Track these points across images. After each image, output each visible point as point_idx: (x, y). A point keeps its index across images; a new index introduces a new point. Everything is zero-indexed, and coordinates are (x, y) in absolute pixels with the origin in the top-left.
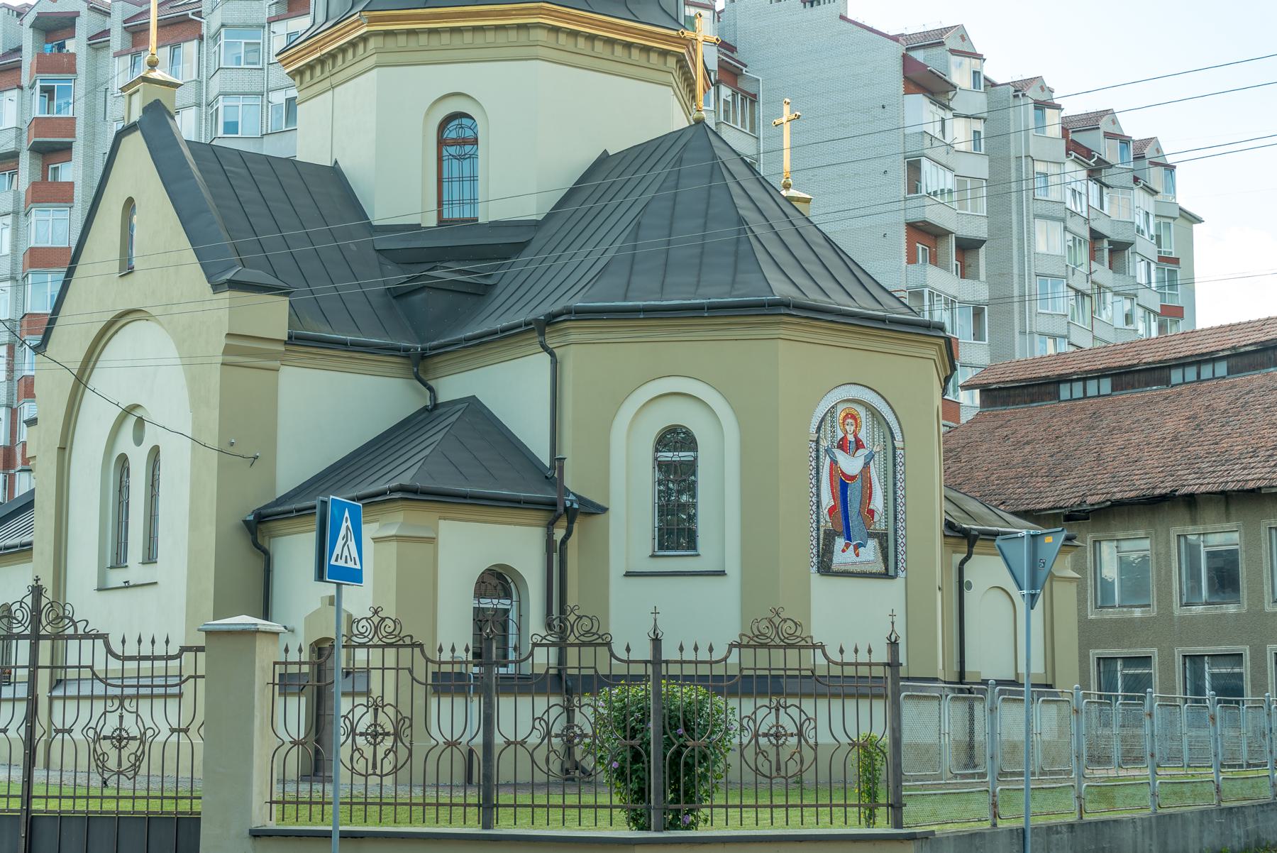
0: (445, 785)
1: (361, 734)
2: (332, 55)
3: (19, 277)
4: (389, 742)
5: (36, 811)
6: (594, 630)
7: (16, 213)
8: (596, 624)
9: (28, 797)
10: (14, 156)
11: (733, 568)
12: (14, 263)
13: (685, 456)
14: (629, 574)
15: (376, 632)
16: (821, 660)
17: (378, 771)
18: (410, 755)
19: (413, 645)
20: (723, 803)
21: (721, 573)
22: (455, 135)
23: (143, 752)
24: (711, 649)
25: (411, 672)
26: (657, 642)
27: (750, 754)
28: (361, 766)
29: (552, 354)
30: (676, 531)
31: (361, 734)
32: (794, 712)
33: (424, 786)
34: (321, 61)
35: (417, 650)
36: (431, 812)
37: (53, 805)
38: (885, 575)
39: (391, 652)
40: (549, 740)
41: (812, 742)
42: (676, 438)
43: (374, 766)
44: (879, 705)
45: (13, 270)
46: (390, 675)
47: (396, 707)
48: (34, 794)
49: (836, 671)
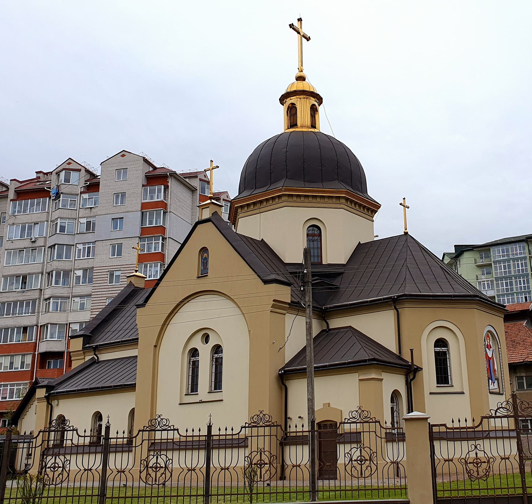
2: (261, 202)
4: (162, 470)
5: (439, 498)
6: (167, 424)
8: (369, 413)
9: (524, 487)
11: (466, 391)
13: (444, 349)
14: (431, 393)
15: (360, 416)
16: (177, 436)
17: (363, 476)
18: (171, 475)
19: (174, 430)
21: (463, 393)
22: (315, 233)
23: (489, 467)
24: (232, 429)
25: (276, 436)
26: (210, 427)
27: (348, 468)
28: (355, 473)
29: (397, 311)
30: (443, 376)
32: (164, 457)
34: (254, 204)
35: (176, 432)
37: (447, 494)
38: (499, 394)
39: (267, 429)
40: (147, 469)
41: (375, 462)
42: (441, 343)
43: (361, 474)
44: (306, 449)
46: (267, 438)
47: (270, 452)
48: (527, 486)
49: (184, 439)
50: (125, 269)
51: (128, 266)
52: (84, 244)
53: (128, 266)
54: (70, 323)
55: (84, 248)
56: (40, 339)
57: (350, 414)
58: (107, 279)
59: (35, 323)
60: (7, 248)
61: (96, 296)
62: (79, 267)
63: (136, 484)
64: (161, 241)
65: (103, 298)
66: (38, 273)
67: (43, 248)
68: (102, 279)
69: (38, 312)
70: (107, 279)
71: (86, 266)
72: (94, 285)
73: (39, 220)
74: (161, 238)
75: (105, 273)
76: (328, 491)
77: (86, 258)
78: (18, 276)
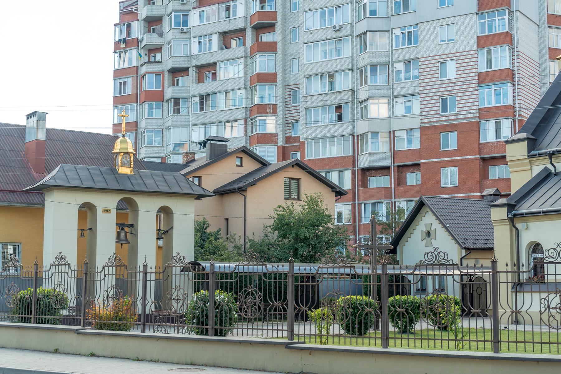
0: (473, 333)
1: (553, 308)
3: (248, 87)
7: (246, 57)
8: (446, 256)
10: (243, 30)
12: (246, 81)
20: (483, 339)
27: (545, 317)
31: (553, 308)
33: (477, 333)
36: (330, 339)
40: (549, 310)
45: (245, 84)
50: (461, 58)
51: (465, 53)
52: (402, 28)
53: (465, 53)
54: (394, 132)
55: (403, 34)
56: (358, 153)
57: (426, 256)
58: (437, 72)
59: (351, 132)
60: (306, 42)
61: (425, 95)
62: (400, 59)
63: (537, 329)
64: (507, 17)
65: (435, 98)
66: (348, 70)
67: (350, 37)
68: (431, 73)
69: (353, 120)
70: (437, 72)
71: (407, 57)
72: (421, 81)
73: (340, 2)
74: (507, 11)
75: (435, 65)
76: (479, 341)
77: (406, 46)
78: (322, 75)
